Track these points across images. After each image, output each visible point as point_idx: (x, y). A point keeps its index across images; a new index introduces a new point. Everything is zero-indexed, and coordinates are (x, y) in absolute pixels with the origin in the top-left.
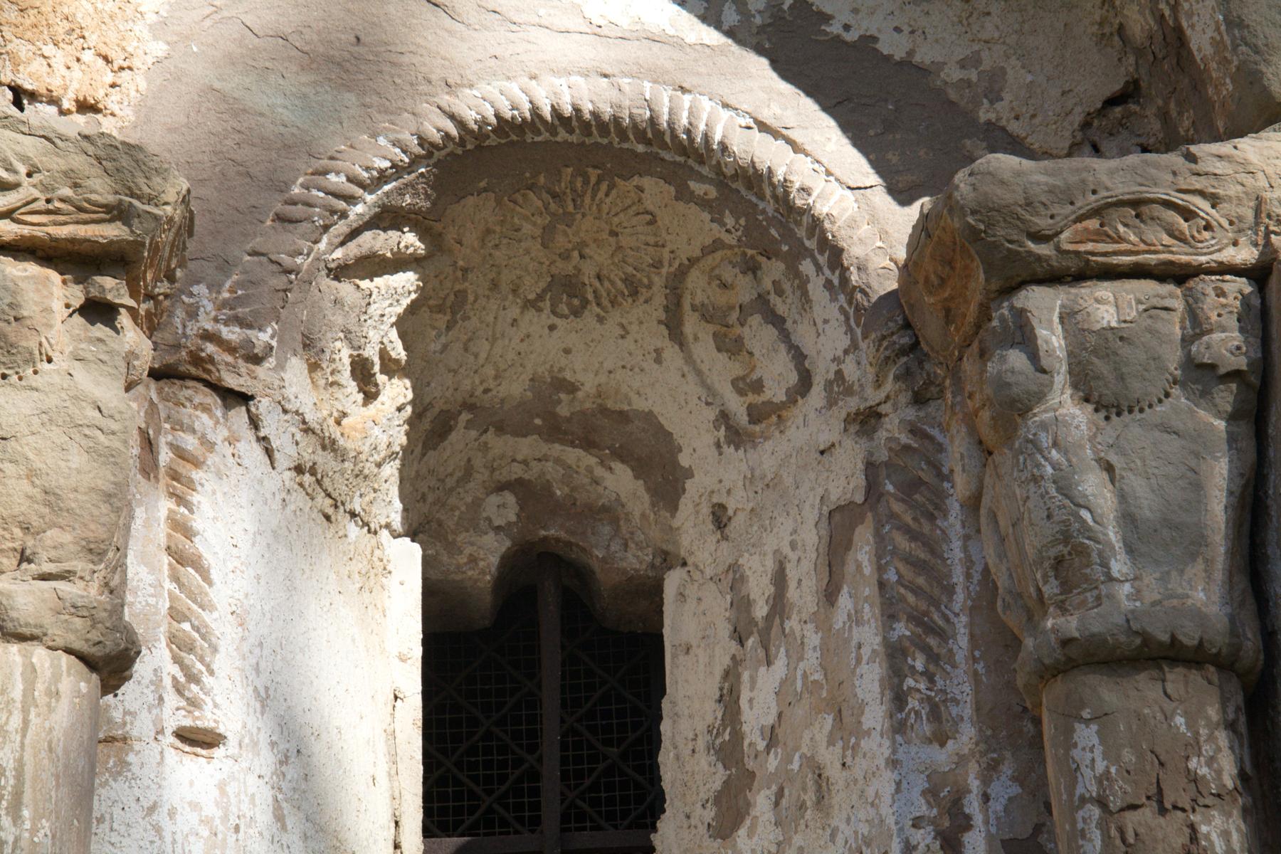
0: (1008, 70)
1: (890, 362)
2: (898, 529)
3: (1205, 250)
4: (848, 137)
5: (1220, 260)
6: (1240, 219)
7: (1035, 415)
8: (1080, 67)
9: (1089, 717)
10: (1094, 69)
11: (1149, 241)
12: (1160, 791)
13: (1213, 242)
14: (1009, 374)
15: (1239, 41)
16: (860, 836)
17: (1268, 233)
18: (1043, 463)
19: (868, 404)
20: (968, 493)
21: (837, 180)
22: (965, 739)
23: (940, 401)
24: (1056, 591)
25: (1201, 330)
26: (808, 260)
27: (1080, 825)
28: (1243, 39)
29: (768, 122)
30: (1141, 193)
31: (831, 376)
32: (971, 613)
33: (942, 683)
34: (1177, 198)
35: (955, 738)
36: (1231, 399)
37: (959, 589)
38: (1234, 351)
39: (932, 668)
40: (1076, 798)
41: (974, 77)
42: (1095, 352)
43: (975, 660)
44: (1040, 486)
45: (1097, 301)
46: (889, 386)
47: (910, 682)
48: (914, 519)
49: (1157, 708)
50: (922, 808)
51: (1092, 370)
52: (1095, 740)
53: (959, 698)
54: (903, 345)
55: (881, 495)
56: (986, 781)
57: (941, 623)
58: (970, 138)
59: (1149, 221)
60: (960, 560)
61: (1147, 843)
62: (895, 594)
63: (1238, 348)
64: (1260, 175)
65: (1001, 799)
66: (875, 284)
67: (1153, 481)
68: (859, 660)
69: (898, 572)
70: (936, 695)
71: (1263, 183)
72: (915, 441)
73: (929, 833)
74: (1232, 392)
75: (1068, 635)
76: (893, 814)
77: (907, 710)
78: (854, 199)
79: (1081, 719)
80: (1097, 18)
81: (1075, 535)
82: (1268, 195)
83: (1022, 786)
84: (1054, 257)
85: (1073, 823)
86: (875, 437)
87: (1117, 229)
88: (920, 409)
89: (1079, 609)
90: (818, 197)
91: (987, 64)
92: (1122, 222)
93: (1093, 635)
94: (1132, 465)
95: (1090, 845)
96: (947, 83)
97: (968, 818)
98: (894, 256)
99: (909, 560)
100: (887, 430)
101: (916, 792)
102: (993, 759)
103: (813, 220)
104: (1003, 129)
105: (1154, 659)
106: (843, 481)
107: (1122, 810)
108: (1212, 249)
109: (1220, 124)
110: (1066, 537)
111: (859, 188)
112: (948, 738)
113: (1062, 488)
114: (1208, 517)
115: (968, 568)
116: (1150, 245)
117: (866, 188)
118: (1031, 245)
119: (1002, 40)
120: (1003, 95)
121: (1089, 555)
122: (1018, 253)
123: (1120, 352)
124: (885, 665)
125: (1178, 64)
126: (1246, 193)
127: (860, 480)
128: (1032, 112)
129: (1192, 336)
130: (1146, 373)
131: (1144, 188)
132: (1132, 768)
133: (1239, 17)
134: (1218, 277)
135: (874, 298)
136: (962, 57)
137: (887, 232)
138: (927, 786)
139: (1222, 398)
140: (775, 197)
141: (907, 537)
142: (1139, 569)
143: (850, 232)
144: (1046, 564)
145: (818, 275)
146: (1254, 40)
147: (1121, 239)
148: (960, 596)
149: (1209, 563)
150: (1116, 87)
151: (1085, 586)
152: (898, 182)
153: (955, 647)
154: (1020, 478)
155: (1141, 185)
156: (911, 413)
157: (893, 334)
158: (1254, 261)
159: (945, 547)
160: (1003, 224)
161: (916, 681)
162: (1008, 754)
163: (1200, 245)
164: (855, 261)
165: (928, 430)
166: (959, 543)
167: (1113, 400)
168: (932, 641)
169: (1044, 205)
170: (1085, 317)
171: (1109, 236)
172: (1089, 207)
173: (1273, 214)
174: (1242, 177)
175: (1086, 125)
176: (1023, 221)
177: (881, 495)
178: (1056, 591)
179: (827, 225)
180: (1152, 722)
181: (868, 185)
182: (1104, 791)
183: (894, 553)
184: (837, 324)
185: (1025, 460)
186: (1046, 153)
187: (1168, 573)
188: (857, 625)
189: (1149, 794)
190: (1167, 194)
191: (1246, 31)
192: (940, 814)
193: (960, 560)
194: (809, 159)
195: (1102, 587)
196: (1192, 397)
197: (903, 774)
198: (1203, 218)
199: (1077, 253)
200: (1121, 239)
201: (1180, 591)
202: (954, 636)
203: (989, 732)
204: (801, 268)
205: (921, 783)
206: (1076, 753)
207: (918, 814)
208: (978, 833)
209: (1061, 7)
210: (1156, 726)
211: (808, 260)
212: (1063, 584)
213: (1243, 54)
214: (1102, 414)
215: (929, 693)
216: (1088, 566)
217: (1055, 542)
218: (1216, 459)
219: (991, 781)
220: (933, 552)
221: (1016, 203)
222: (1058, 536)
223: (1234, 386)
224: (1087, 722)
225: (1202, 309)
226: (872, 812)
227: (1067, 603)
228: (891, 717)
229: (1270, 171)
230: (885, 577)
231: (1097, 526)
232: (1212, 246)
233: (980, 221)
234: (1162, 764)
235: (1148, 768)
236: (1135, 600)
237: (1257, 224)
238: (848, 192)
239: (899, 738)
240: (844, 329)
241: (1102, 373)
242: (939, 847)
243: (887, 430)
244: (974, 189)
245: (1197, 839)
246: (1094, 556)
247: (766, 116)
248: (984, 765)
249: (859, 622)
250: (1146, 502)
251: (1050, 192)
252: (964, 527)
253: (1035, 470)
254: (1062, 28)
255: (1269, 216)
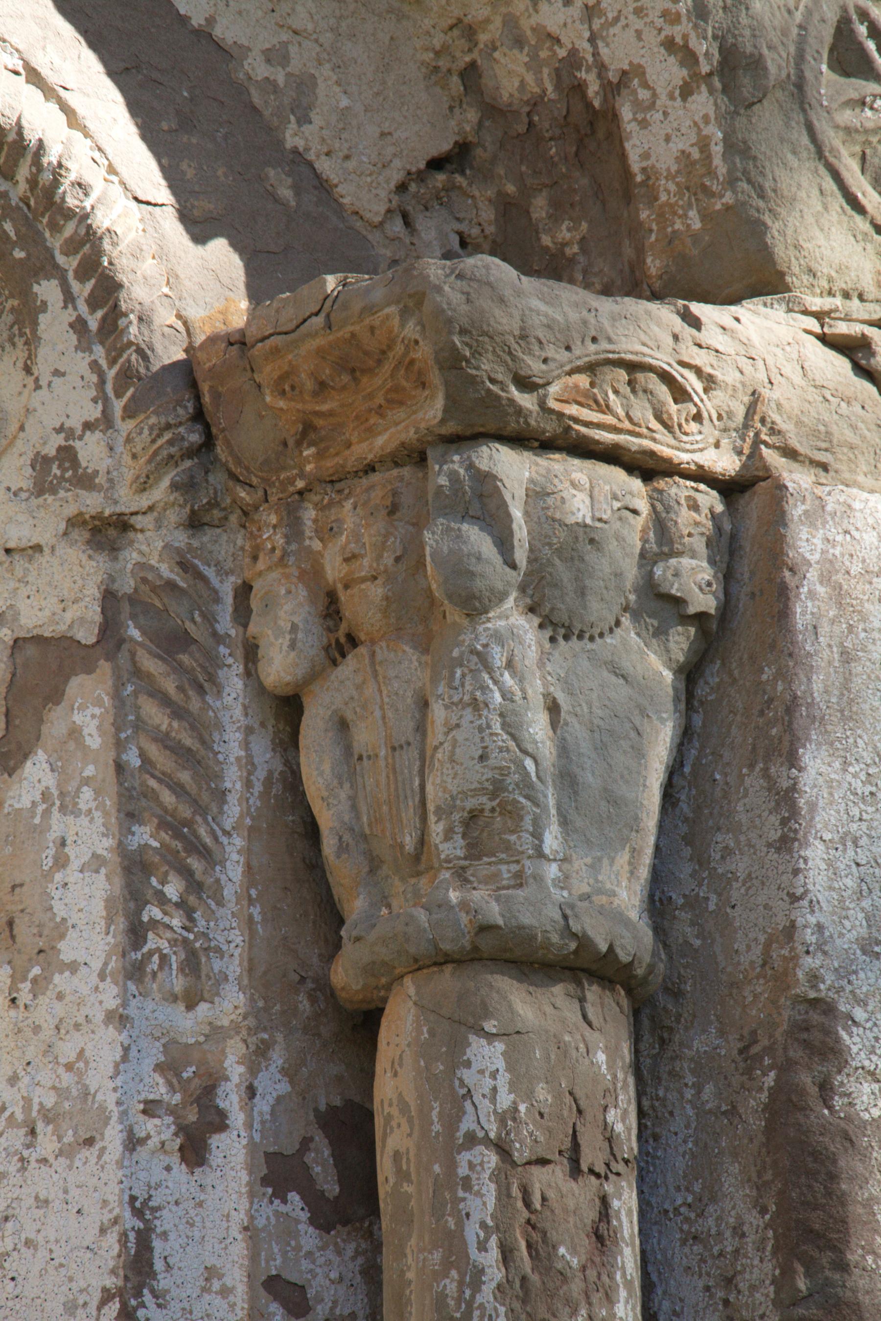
0: (319, 81)
1: (173, 462)
2: (151, 695)
3: (688, 446)
4: (137, 125)
5: (702, 463)
6: (730, 414)
7: (489, 620)
8: (403, 104)
9: (494, 1031)
10: (419, 112)
11: (636, 420)
12: (576, 1146)
13: (699, 437)
14: (474, 560)
15: (739, 174)
16: (36, 1107)
17: (757, 442)
18: (491, 686)
19: (119, 509)
20: (288, 678)
21: (123, 183)
22: (227, 1006)
23: (218, 531)
24: (460, 853)
25: (671, 550)
26: (54, 282)
27: (463, 1171)
28: (745, 172)
29: (45, 71)
30: (644, 355)
31: (50, 450)
32: (249, 836)
33: (204, 923)
34: (677, 372)
35: (212, 1003)
36: (685, 646)
37: (233, 799)
38: (704, 586)
39: (192, 900)
40: (460, 1134)
41: (281, 80)
42: (559, 552)
43: (251, 901)
44: (480, 716)
45: (573, 485)
46: (160, 492)
47: (153, 912)
48: (180, 689)
49: (579, 1037)
50: (160, 1090)
51: (551, 574)
52: (501, 1064)
53: (225, 948)
54: (192, 444)
55: (121, 642)
56: (253, 1070)
57: (208, 840)
58: (274, 168)
59: (640, 393)
60: (238, 759)
61: (556, 1211)
62: (136, 785)
63: (709, 584)
64: (760, 364)
65: (268, 1097)
66: (159, 348)
67: (597, 735)
68: (61, 862)
69: (142, 755)
70: (196, 939)
71: (762, 376)
72: (183, 579)
73: (168, 1127)
74: (688, 638)
75: (492, 922)
76: (115, 1090)
77: (145, 950)
78: (139, 216)
79: (482, 1032)
80: (437, 43)
81: (510, 788)
82: (766, 392)
83: (291, 1082)
84: (535, 415)
85: (452, 1165)
86: (121, 557)
87: (607, 395)
88: (193, 535)
89: (486, 883)
90: (99, 200)
91: (295, 65)
92: (613, 386)
93: (521, 927)
94: (578, 709)
95: (478, 1201)
96: (250, 78)
97: (222, 1115)
98: (183, 313)
99: (164, 740)
100: (141, 552)
101: (148, 1064)
102: (263, 1041)
103: (88, 233)
104: (310, 164)
105: (571, 969)
106: (51, 604)
107: (529, 1163)
108: (696, 447)
109: (653, 265)
110: (497, 788)
111: (148, 203)
112: (202, 999)
113: (509, 726)
114: (645, 795)
115: (250, 773)
116: (635, 424)
117: (155, 205)
118: (515, 393)
119: (315, 36)
120: (313, 115)
121: (521, 818)
122: (498, 398)
123: (587, 558)
124: (118, 881)
125: (577, 154)
126: (743, 384)
127: (94, 613)
128: (346, 152)
129: (656, 555)
130: (605, 592)
131: (645, 350)
132: (547, 1110)
133: (745, 142)
134: (693, 484)
135: (156, 367)
136: (267, 46)
137: (177, 277)
138: (163, 1059)
139: (677, 643)
140: (33, 183)
141: (168, 711)
142: (570, 847)
143: (133, 263)
144: (456, 816)
145: (65, 307)
146: (760, 179)
147: (607, 409)
148: (233, 810)
149: (635, 852)
150: (445, 146)
151: (503, 856)
152: (193, 206)
153: (223, 878)
154: (450, 697)
155: (644, 344)
156: (181, 539)
157: (180, 424)
158: (733, 474)
159: (216, 736)
160: (490, 356)
161: (165, 913)
162: (279, 1037)
163: (685, 438)
164: (138, 307)
165: (202, 568)
166: (239, 736)
167: (565, 618)
168: (195, 864)
169: (541, 343)
170: (559, 503)
171: (596, 402)
172: (587, 359)
173: (769, 420)
174: (744, 363)
175: (402, 188)
176: (514, 358)
177: (121, 642)
178: (460, 853)
179: (106, 245)
180: (574, 1053)
181: (160, 202)
182: (508, 1134)
183: (139, 725)
184: (80, 383)
185: (463, 676)
186: (357, 213)
187: (600, 859)
188: (63, 809)
189: (563, 1148)
190: (669, 364)
191: (751, 163)
192: (184, 1102)
193: (238, 759)
194: (88, 141)
195: (527, 863)
196: (644, 633)
197: (134, 1038)
198: (696, 405)
199: (560, 415)
200: (607, 409)
201: (608, 886)
202: (222, 863)
203: (261, 1004)
204: (36, 288)
205: (154, 1053)
206: (467, 1074)
207: (151, 1097)
208: (235, 1137)
209: (388, 12)
210: (577, 1061)
211: (54, 282)
212: (470, 846)
213: (743, 192)
214: (548, 633)
215: (185, 934)
216: (513, 832)
217: (480, 791)
218: (663, 721)
219: (259, 1071)
220: (203, 742)
221: (511, 333)
222: (487, 785)
223: (692, 630)
224: (490, 1037)
225: (676, 523)
226: (67, 1079)
227: (469, 872)
228: (124, 955)
229: (770, 362)
230: (124, 757)
231: (539, 783)
232: (697, 442)
233: (467, 344)
234: (580, 1111)
235: (566, 1113)
236: (562, 888)
237: (746, 426)
238: (134, 204)
239: (132, 987)
240: (93, 393)
241: (561, 580)
242: (177, 1147)
243: (141, 552)
244: (468, 301)
245: (607, 1216)
246: (528, 820)
247: (40, 63)
248: (252, 1048)
249: (68, 808)
250: (589, 762)
251: (549, 327)
252: (246, 715)
253: (478, 694)
254: (387, 42)
255: (763, 421)
